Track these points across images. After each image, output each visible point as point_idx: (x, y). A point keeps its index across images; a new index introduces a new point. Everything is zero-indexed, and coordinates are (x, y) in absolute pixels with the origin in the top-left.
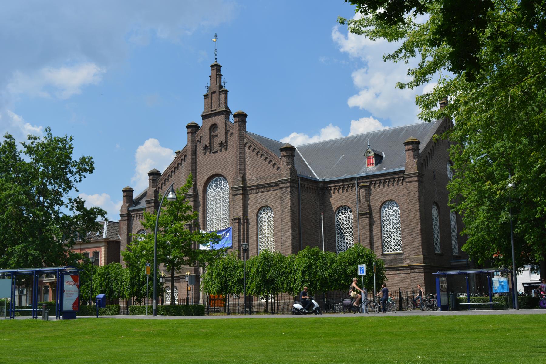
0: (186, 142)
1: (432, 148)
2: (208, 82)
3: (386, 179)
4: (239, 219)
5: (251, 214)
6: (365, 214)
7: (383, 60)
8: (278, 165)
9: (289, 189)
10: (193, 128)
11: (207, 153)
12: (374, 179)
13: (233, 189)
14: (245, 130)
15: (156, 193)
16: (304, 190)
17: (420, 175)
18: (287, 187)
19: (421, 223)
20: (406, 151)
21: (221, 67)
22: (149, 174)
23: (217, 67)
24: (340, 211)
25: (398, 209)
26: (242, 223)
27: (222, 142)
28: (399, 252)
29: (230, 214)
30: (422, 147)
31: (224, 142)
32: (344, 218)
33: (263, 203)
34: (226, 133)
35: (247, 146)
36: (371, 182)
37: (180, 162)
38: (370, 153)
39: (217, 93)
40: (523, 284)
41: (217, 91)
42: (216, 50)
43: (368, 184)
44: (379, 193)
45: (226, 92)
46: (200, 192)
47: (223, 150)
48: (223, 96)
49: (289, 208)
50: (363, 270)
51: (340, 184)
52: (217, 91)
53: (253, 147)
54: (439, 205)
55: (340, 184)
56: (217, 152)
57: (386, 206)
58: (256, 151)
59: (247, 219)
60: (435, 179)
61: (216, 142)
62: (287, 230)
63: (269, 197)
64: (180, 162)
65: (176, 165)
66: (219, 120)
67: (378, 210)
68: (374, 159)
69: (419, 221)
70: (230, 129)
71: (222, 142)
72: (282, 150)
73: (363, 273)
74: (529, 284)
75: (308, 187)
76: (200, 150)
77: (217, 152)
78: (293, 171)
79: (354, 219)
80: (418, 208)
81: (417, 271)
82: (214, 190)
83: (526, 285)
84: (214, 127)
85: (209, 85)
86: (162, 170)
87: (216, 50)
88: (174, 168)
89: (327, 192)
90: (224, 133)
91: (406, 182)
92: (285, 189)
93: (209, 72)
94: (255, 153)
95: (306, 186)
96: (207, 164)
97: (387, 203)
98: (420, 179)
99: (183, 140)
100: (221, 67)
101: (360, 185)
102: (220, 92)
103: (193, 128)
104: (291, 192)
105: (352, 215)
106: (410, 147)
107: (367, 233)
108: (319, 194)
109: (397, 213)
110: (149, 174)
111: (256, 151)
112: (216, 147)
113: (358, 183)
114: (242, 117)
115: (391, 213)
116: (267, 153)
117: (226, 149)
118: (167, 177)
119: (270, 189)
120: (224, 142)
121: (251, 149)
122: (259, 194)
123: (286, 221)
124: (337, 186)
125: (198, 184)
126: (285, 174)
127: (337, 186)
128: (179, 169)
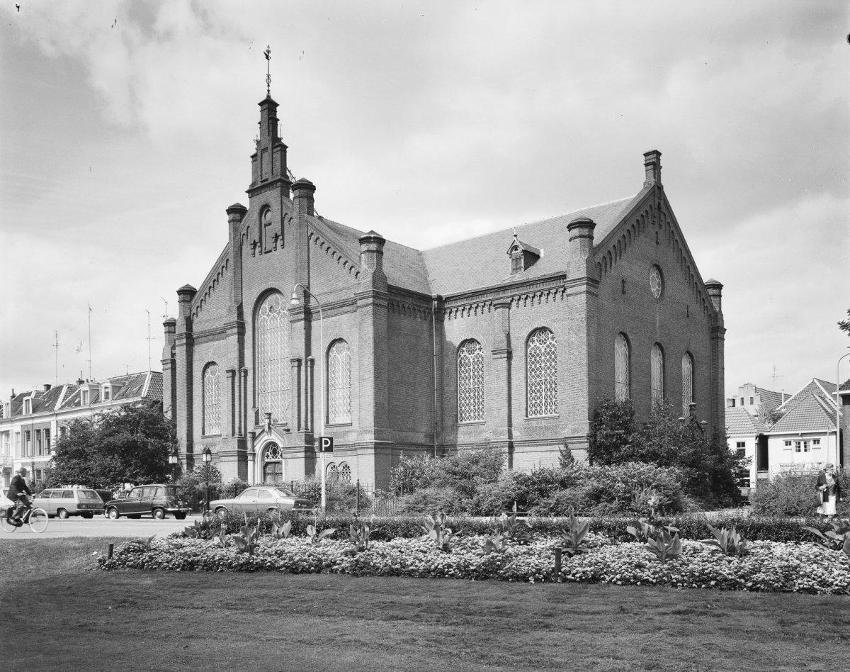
0: (227, 241)
1: (621, 239)
4: (299, 361)
5: (318, 352)
7: (798, 453)
9: (370, 308)
10: (237, 212)
14: (310, 210)
15: (189, 322)
17: (593, 282)
18: (367, 305)
19: (589, 365)
20: (570, 240)
21: (278, 105)
22: (178, 292)
23: (269, 106)
27: (276, 234)
30: (599, 235)
35: (313, 238)
36: (513, 297)
38: (516, 250)
39: (270, 151)
41: (272, 145)
42: (269, 76)
43: (508, 300)
45: (284, 148)
46: (248, 318)
48: (278, 156)
49: (371, 341)
52: (272, 145)
53: (321, 240)
54: (630, 337)
58: (325, 246)
59: (312, 361)
60: (624, 292)
61: (270, 232)
62: (367, 377)
63: (344, 324)
65: (215, 277)
66: (272, 196)
67: (523, 346)
69: (585, 361)
72: (362, 241)
76: (247, 249)
77: (271, 251)
78: (379, 277)
80: (585, 340)
84: (265, 208)
85: (259, 138)
87: (269, 76)
88: (214, 280)
90: (279, 218)
91: (568, 295)
93: (256, 114)
96: (260, 273)
98: (592, 290)
99: (220, 234)
100: (278, 105)
102: (273, 148)
103: (237, 212)
104: (375, 313)
106: (576, 232)
107: (504, 384)
110: (178, 292)
111: (325, 246)
112: (269, 244)
114: (307, 188)
116: (334, 244)
120: (279, 233)
126: (366, 283)
128: (212, 296)
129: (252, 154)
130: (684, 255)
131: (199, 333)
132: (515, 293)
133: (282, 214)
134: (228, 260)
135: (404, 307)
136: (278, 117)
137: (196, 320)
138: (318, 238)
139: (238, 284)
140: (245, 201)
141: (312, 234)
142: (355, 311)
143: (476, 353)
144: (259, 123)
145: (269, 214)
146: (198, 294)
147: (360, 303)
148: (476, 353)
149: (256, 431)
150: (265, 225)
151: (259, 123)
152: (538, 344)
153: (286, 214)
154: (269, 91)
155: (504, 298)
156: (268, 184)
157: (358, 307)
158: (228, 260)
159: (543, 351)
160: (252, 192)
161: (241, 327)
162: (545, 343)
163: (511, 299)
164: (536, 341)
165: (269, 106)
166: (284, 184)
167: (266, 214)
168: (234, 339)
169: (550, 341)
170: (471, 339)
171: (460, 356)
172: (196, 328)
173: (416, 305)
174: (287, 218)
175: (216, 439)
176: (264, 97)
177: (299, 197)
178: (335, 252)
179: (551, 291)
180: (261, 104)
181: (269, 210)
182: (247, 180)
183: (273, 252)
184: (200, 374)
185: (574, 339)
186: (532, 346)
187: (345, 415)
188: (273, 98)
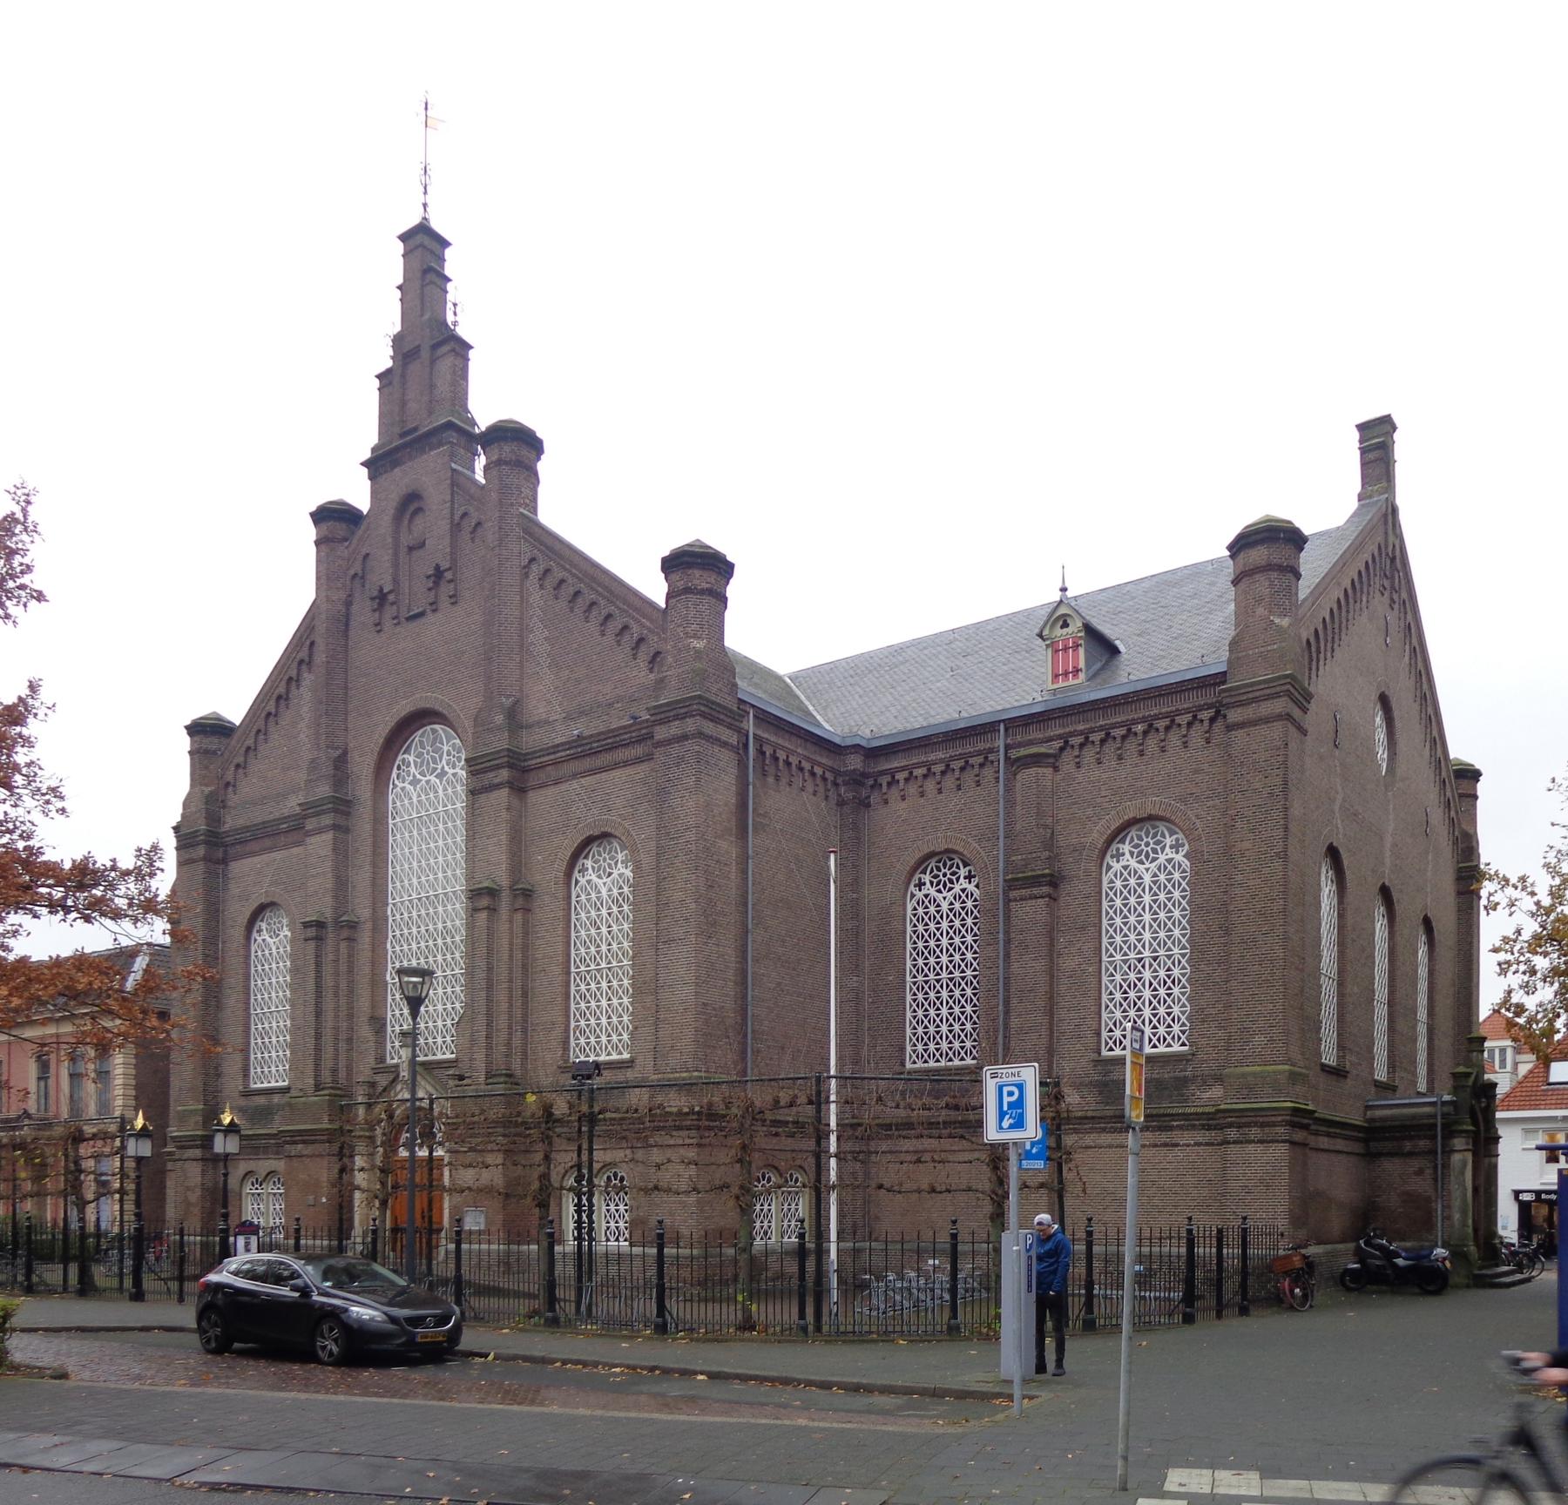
2: (390, 319)
3: (1135, 722)
6: (1035, 881)
8: (654, 642)
11: (388, 624)
12: (1081, 727)
13: (475, 766)
16: (771, 770)
19: (1198, 984)
23: (424, 250)
24: (927, 878)
25: (1179, 857)
26: (510, 906)
27: (437, 567)
28: (1176, 1048)
29: (470, 877)
31: (445, 565)
32: (945, 906)
33: (589, 819)
34: (456, 528)
35: (536, 570)
36: (1065, 738)
37: (294, 673)
38: (1065, 625)
40: (1517, 1193)
41: (428, 352)
44: (1097, 782)
47: (444, 602)
50: (1019, 1104)
51: (932, 757)
52: (428, 352)
53: (559, 574)
55: (932, 757)
56: (421, 614)
57: (1126, 848)
63: (614, 792)
64: (294, 673)
65: (282, 690)
68: (1081, 651)
70: (471, 510)
71: (437, 567)
73: (1019, 1124)
74: (1538, 1193)
75: (794, 760)
76: (363, 612)
77: (421, 614)
79: (984, 910)
81: (1255, 1132)
82: (415, 782)
83: (1525, 1197)
84: (411, 504)
86: (235, 714)
88: (276, 697)
89: (875, 798)
92: (675, 750)
93: (392, 266)
94: (562, 604)
95: (782, 755)
97: (1133, 833)
100: (445, 244)
101: (1014, 754)
105: (977, 893)
108: (841, 803)
109: (1177, 876)
110: (187, 727)
113: (1007, 747)
115: (1147, 879)
117: (454, 599)
118: (250, 742)
119: (621, 754)
121: (550, 582)
122: (575, 784)
123: (679, 895)
124: (918, 765)
125: (354, 757)
127: (918, 765)
129: (382, 369)
130: (1420, 665)
131: (238, 831)
132: (1071, 729)
133: (452, 514)
134: (312, 644)
135: (777, 759)
136: (448, 272)
137: (233, 799)
138: (547, 571)
139: (336, 704)
140: (359, 495)
141: (532, 560)
142: (649, 757)
143: (1162, 858)
144: (399, 288)
145: (419, 520)
146: (236, 736)
147: (661, 733)
148: (1162, 858)
149: (378, 1078)
150: (411, 549)
151: (399, 288)
152: (933, 892)
153: (465, 515)
154: (425, 205)
155: (1043, 741)
156: (420, 438)
157: (659, 744)
158: (312, 644)
159: (1147, 879)
160: (377, 465)
161: (342, 806)
162: (1154, 859)
163: (1057, 744)
164: (1128, 856)
165: (424, 250)
166: (462, 435)
167: (410, 521)
168: (321, 844)
169: (964, 883)
170: (947, 851)
171: (1109, 867)
172: (230, 822)
173: (808, 759)
174: (468, 525)
175: (276, 1099)
176: (415, 221)
177: (499, 462)
178: (593, 604)
179: (1178, 719)
180: (404, 238)
181: (419, 510)
182: (366, 435)
183: (430, 618)
184: (237, 933)
185: (1247, 845)
186: (1117, 867)
187: (810, 787)
188: (437, 225)
